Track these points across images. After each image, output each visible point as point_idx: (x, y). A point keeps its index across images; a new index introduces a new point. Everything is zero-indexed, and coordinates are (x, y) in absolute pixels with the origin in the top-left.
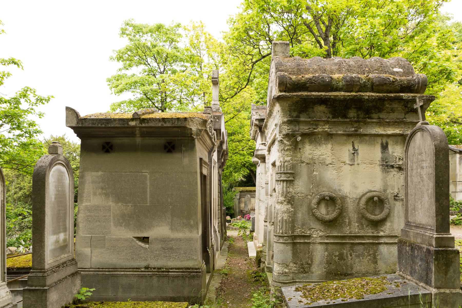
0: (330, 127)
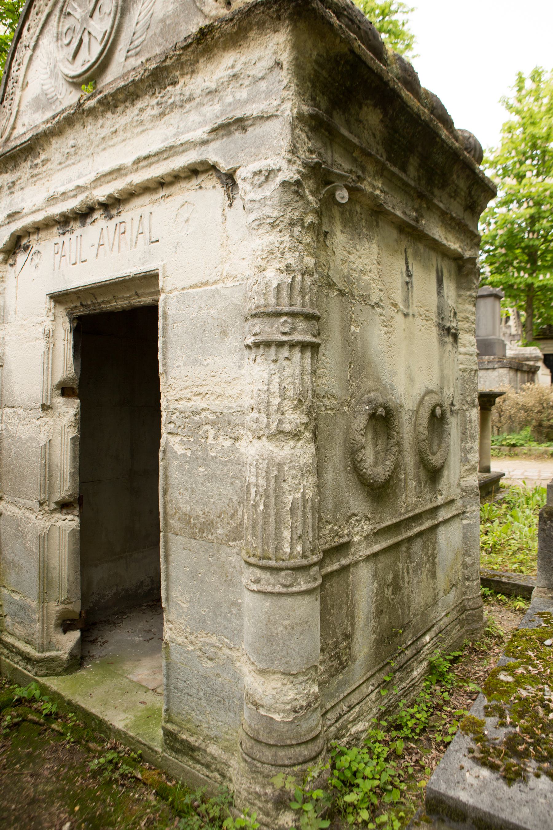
0: (386, 189)
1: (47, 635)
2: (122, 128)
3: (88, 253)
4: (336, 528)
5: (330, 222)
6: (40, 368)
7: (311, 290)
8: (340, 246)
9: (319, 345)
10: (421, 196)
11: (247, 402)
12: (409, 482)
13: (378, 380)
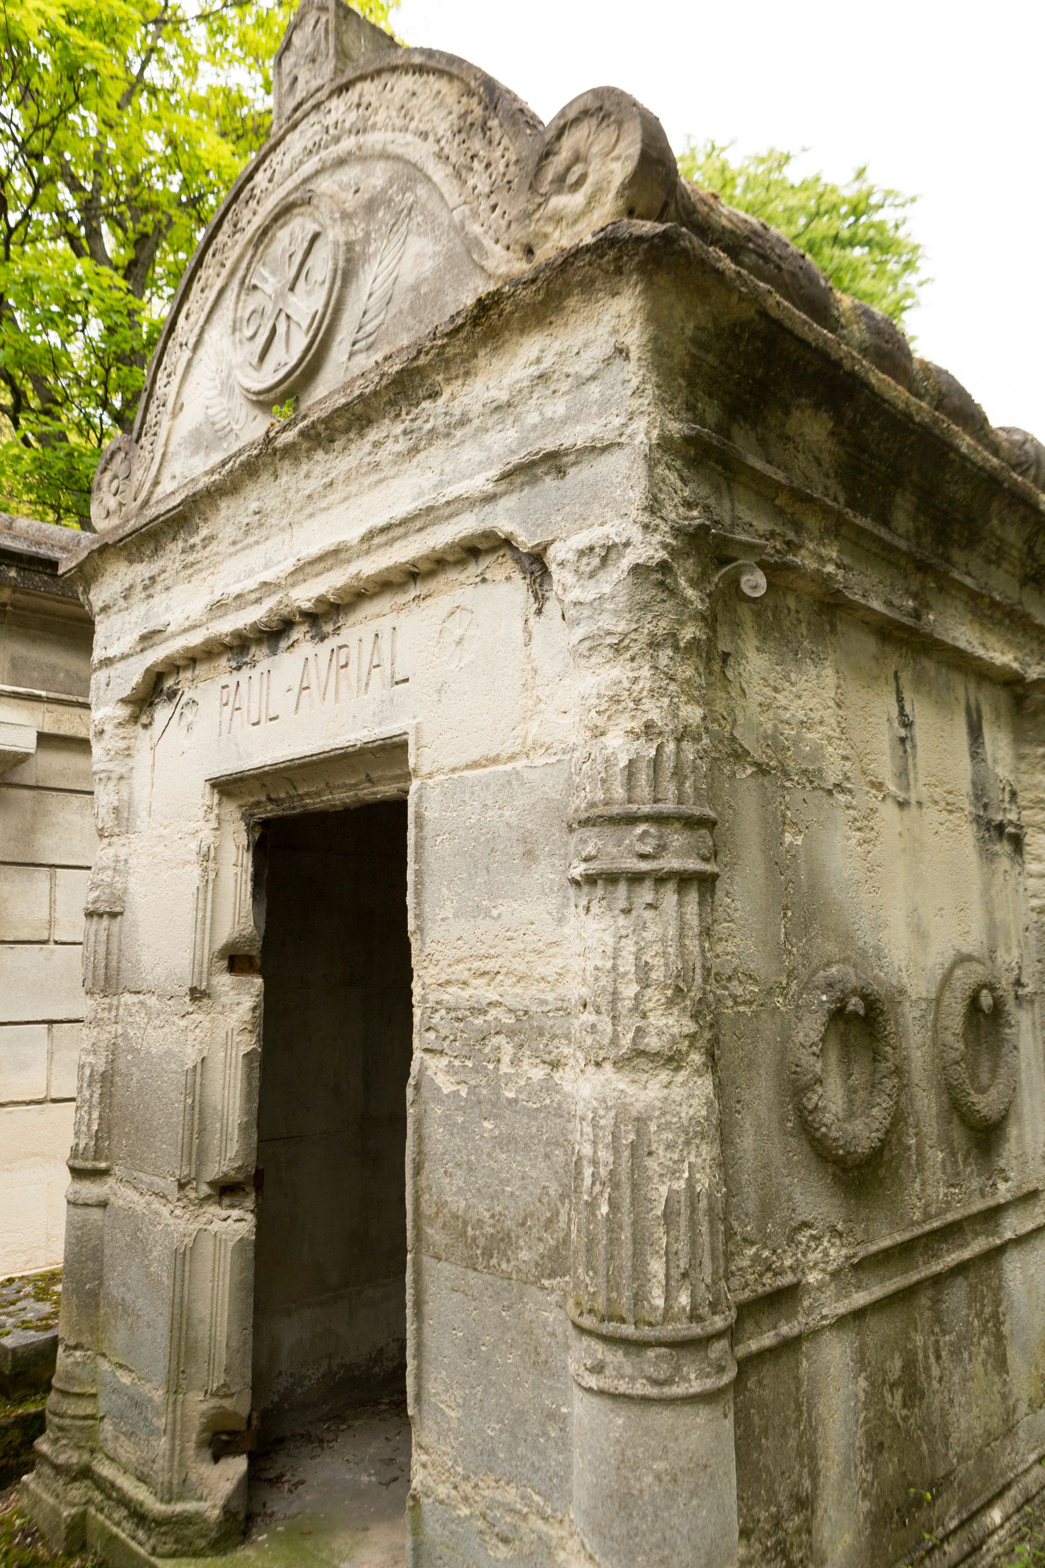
1: (182, 1465)
2: (342, 477)
3: (281, 703)
4: (766, 1253)
5: (733, 633)
6: (190, 918)
7: (695, 769)
8: (756, 677)
9: (714, 877)
10: (923, 567)
11: (575, 990)
12: (929, 1153)
13: (847, 938)
